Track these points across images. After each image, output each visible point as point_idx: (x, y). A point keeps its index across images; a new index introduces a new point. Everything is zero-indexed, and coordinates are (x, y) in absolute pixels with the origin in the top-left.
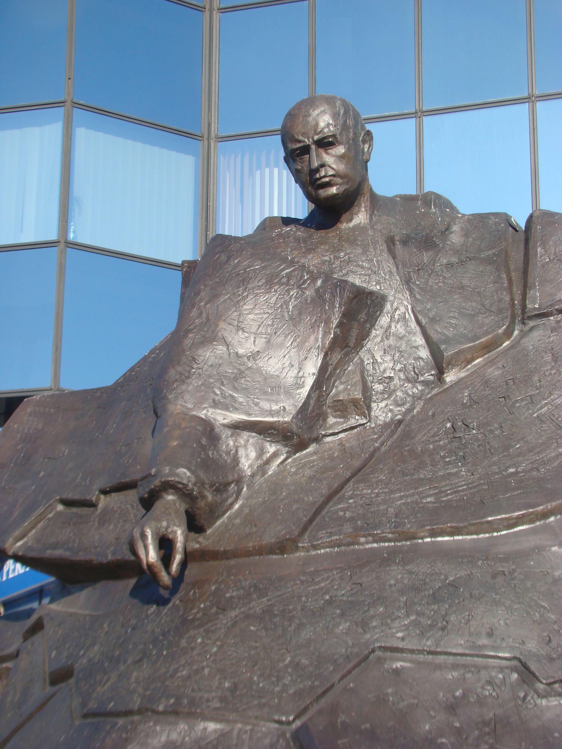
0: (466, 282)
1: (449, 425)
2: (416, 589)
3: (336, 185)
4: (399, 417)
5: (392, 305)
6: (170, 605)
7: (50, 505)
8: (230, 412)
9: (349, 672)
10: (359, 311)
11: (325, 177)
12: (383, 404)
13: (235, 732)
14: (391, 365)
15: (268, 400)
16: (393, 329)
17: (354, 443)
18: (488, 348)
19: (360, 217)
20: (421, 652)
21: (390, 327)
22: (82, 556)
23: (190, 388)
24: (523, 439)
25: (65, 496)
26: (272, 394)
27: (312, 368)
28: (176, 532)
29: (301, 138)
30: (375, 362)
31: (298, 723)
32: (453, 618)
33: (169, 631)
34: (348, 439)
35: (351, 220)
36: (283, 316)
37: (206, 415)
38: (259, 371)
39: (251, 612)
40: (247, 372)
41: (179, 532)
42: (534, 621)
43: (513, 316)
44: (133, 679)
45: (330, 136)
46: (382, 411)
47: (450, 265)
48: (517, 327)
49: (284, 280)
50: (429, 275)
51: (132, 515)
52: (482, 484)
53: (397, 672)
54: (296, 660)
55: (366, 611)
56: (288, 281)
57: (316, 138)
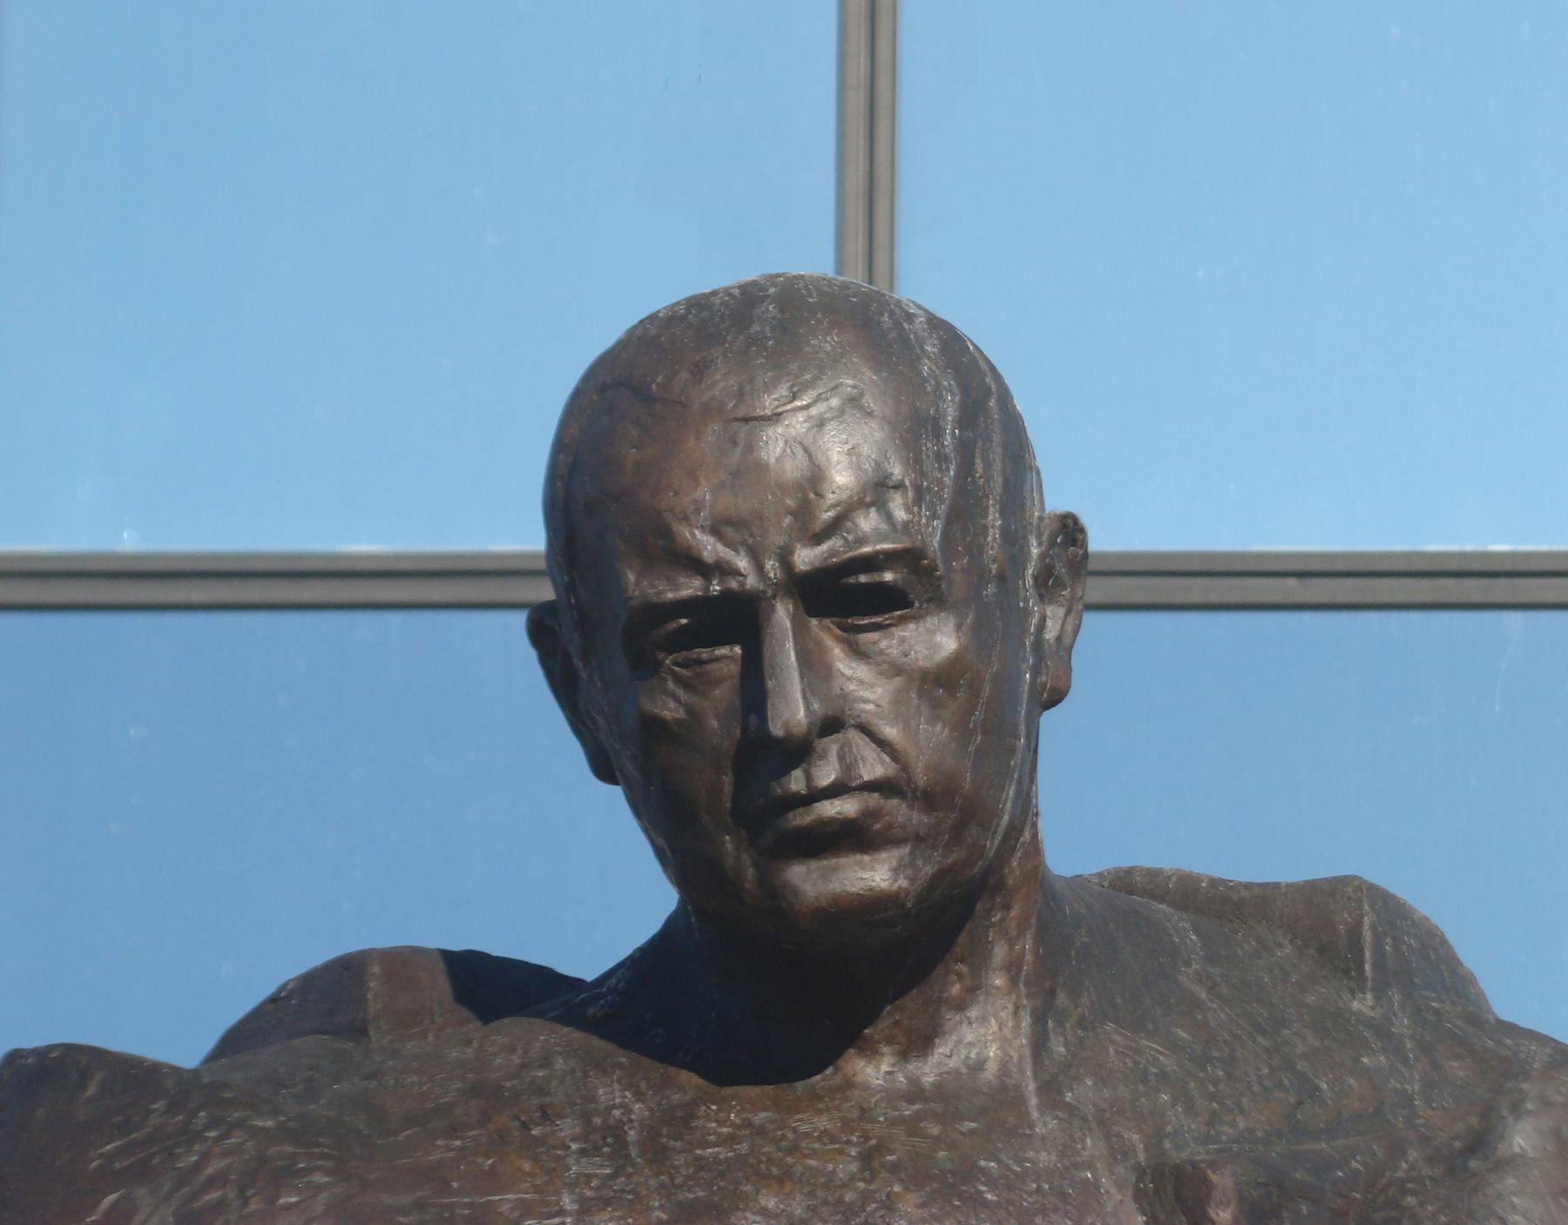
3: (896, 842)
19: (983, 1036)
29: (710, 547)
35: (919, 1042)
57: (806, 557)
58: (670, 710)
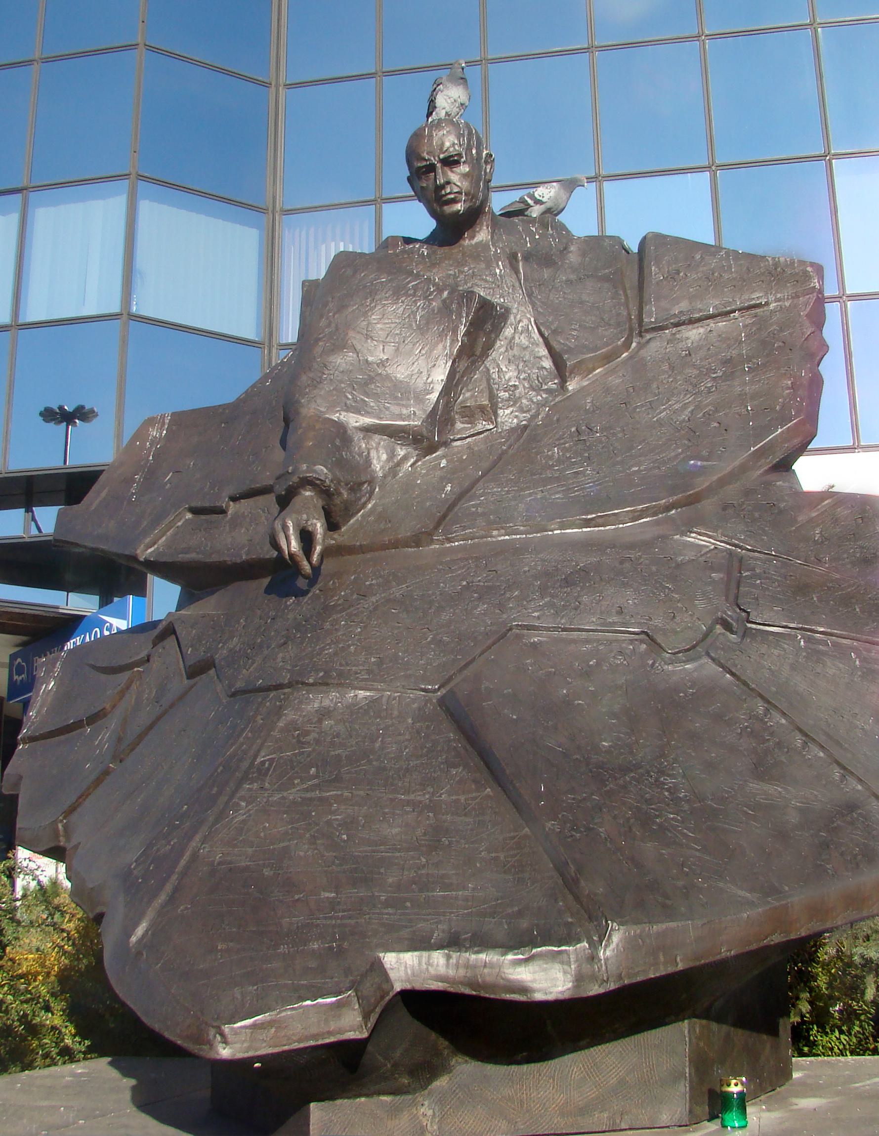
0: (585, 297)
1: (573, 429)
2: (547, 574)
4: (524, 423)
5: (515, 318)
6: (310, 595)
7: (180, 513)
8: (362, 415)
9: (489, 647)
10: (485, 323)
11: (450, 193)
12: (507, 412)
13: (384, 700)
14: (516, 374)
15: (398, 405)
16: (517, 340)
17: (483, 446)
18: (608, 358)
19: (482, 235)
20: (555, 629)
21: (513, 338)
22: (215, 558)
23: (322, 393)
24: (644, 440)
25: (194, 504)
26: (402, 399)
27: (440, 375)
28: (316, 525)
30: (500, 371)
31: (443, 691)
32: (585, 599)
33: (312, 616)
34: (476, 443)
35: (473, 237)
36: (411, 325)
37: (338, 418)
38: (388, 377)
39: (392, 597)
40: (377, 378)
41: (319, 525)
42: (659, 601)
43: (631, 330)
44: (279, 659)
45: (456, 155)
46: (508, 417)
47: (569, 282)
48: (634, 340)
49: (411, 292)
50: (550, 291)
51: (263, 518)
52: (606, 482)
53: (534, 645)
54: (438, 638)
55: (502, 595)
56: (415, 293)
57: (442, 156)
58: (425, 185)
